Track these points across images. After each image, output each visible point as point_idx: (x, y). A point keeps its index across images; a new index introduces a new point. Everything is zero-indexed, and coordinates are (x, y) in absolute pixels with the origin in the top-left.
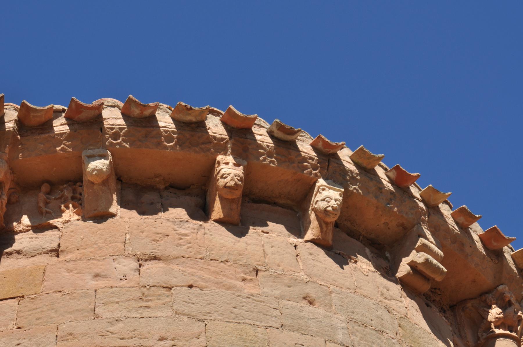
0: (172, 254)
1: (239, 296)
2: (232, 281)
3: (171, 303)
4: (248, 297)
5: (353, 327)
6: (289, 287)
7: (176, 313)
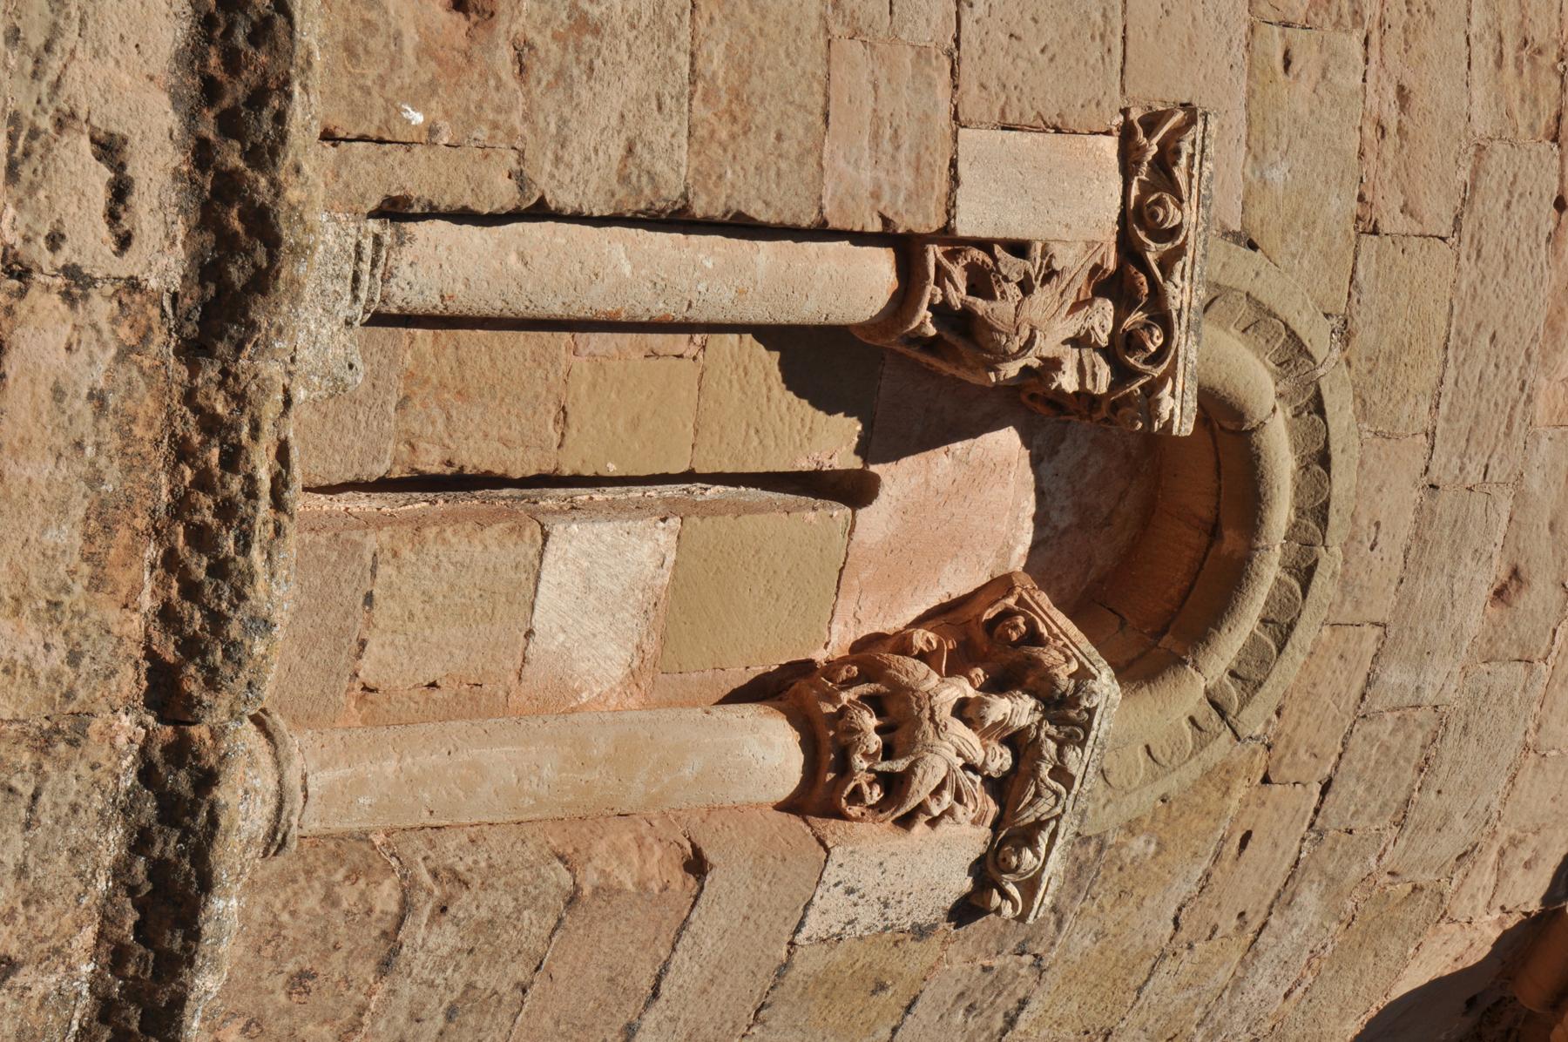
1: (1528, 356)
3: (1510, 134)
4: (1524, 383)
5: (1421, 726)
6: (1552, 526)
7: (1480, 148)
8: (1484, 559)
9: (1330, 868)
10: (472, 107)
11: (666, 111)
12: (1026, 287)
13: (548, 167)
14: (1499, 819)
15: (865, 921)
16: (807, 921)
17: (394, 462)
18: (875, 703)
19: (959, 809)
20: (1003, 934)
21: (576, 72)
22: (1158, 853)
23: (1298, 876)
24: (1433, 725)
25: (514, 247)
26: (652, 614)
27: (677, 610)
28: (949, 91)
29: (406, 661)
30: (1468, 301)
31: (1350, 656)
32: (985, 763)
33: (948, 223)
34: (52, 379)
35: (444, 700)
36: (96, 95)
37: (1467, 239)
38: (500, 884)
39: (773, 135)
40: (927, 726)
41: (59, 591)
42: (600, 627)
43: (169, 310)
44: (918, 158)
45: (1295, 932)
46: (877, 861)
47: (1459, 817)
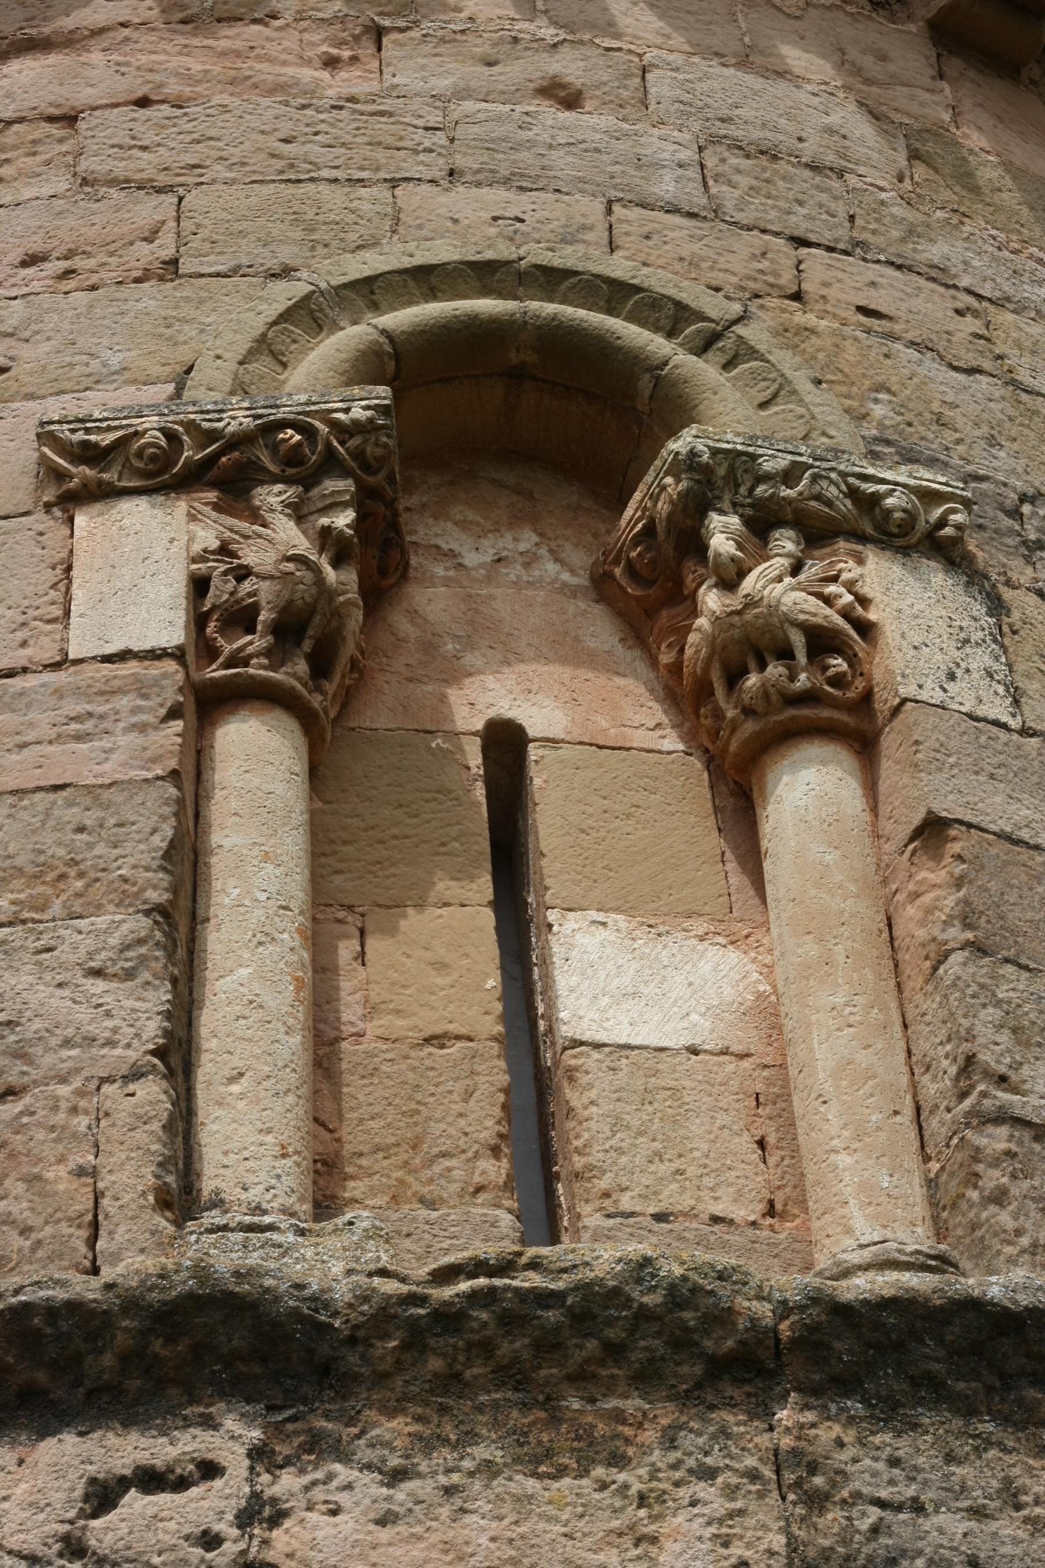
0: (85, 23)
1: (304, 107)
2: (290, 71)
3: (69, 159)
4: (334, 107)
5: (723, 160)
6: (490, 64)
7: (85, 182)
8: (529, 119)
9: (895, 234)
10: (54, 1135)
11: (53, 942)
12: (243, 573)
13: (118, 1051)
14: (827, 83)
15: (988, 661)
16: (991, 716)
17: (498, 1206)
18: (734, 677)
19: (845, 576)
20: (996, 531)
21: (13, 1038)
22: (889, 391)
23: (908, 262)
24: (719, 149)
25: (222, 1089)
26: (661, 929)
27: (651, 906)
28: (29, 676)
29: (733, 1174)
30: (248, 168)
31: (646, 229)
32: (787, 555)
33: (171, 656)
34: (372, 1527)
35: (777, 1130)
36: (41, 1517)
37: (181, 179)
38: (965, 1023)
39: (79, 836)
40: (749, 616)
41: (626, 1497)
42: (678, 979)
43: (290, 1412)
44: (102, 693)
45: (976, 263)
46: (913, 652)
47: (827, 120)
